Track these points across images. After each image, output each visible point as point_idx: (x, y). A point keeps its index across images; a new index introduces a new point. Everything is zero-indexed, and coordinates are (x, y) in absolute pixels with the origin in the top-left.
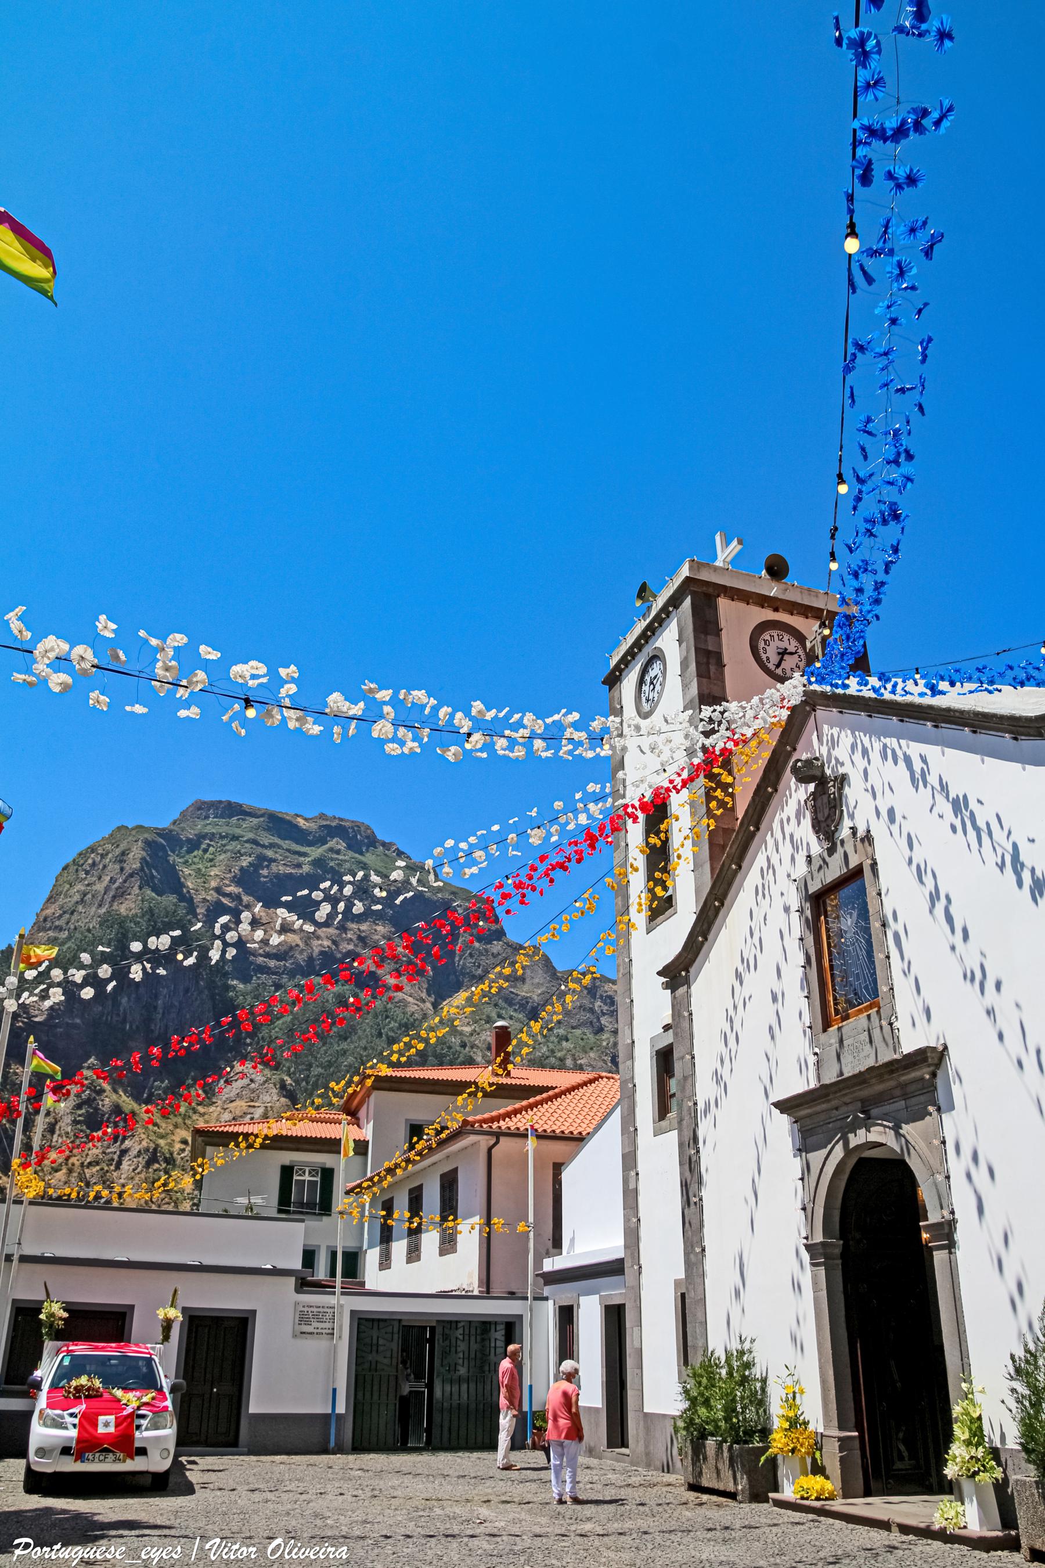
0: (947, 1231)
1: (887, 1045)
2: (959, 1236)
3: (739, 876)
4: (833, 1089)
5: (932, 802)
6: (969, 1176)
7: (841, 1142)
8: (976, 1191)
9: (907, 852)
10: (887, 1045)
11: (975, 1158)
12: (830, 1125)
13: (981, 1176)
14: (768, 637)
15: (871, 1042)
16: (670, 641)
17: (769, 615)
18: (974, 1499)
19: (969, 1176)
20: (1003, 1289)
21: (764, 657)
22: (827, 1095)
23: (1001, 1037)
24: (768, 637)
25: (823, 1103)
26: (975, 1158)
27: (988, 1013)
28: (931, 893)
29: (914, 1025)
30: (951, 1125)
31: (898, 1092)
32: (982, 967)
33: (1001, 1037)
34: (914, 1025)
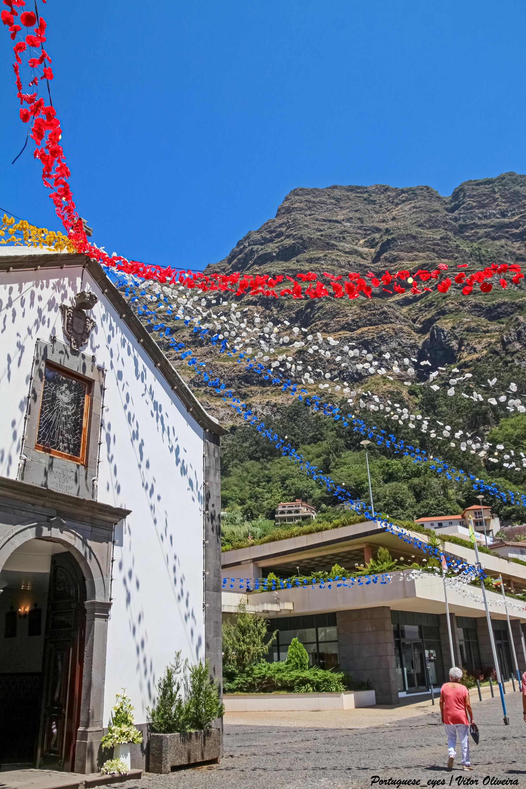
0: (105, 608)
1: (88, 490)
2: (112, 612)
3: (169, 387)
4: (53, 496)
5: (3, 328)
6: (125, 581)
7: (34, 529)
8: (127, 591)
9: (125, 402)
10: (88, 490)
11: (130, 574)
12: (24, 513)
13: (131, 585)
15: (76, 481)
18: (129, 754)
19: (125, 581)
20: (133, 644)
22: (45, 496)
23: (155, 521)
25: (11, 492)
26: (130, 574)
27: (151, 507)
28: (134, 432)
29: (108, 488)
30: (117, 552)
31: (88, 520)
32: (152, 486)
33: (155, 521)
34: (108, 488)
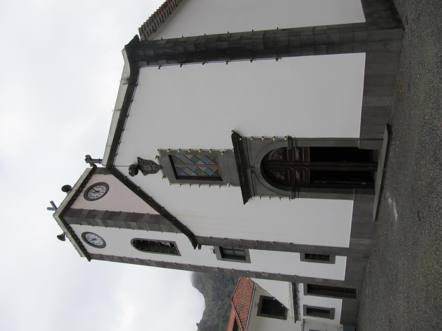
14: (90, 196)
16: (79, 229)
17: (82, 194)
21: (96, 198)
24: (90, 196)
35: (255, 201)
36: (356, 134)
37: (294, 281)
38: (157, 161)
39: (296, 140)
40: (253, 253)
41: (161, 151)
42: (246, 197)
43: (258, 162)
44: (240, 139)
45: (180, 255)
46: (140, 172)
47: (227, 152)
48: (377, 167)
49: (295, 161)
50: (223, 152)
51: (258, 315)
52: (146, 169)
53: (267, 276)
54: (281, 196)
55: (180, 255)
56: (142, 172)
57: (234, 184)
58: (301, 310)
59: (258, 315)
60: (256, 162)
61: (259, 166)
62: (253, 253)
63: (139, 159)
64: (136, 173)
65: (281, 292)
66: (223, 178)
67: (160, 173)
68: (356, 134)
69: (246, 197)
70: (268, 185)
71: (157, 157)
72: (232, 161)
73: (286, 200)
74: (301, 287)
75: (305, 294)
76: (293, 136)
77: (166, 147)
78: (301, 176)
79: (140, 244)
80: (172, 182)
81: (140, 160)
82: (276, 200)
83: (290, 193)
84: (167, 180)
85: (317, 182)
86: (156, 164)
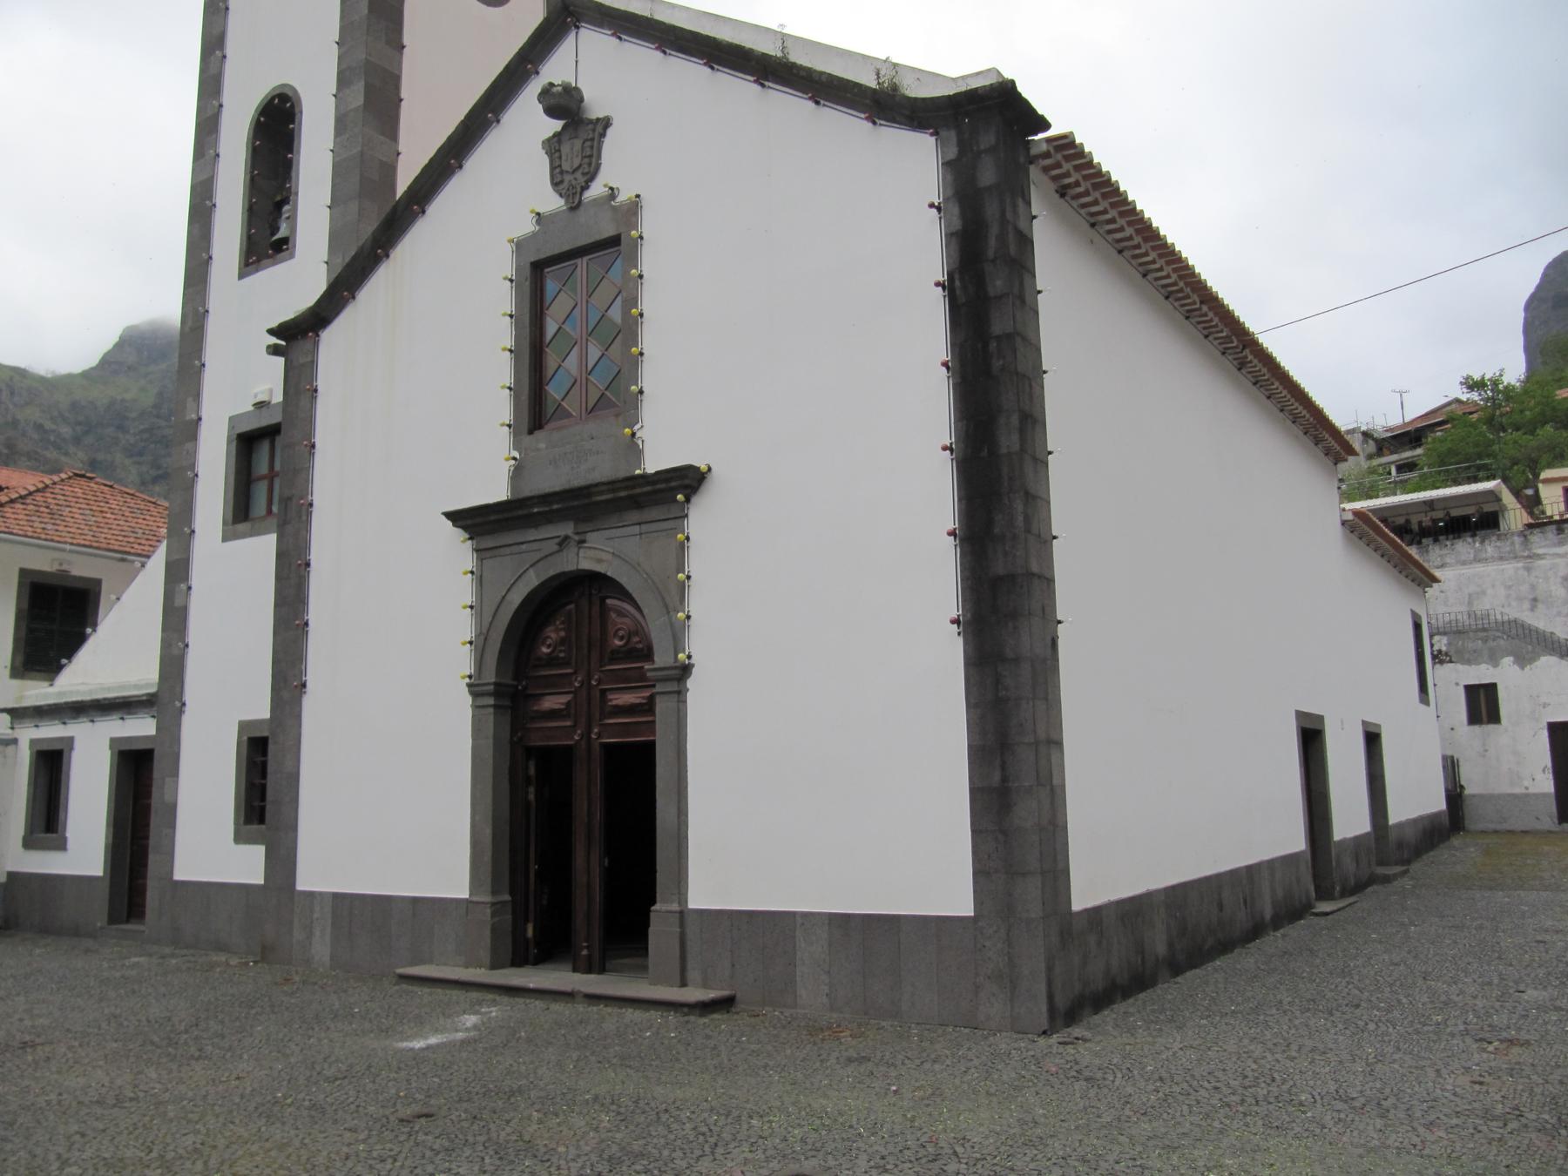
35: (458, 551)
36: (698, 898)
37: (164, 702)
38: (596, 190)
39: (680, 694)
40: (263, 548)
41: (634, 207)
42: (475, 522)
43: (600, 561)
44: (680, 497)
45: (241, 276)
46: (557, 125)
47: (633, 449)
48: (589, 971)
49: (604, 692)
50: (633, 435)
51: (24, 573)
52: (565, 149)
53: (178, 602)
54: (479, 645)
55: (241, 276)
56: (557, 135)
57: (517, 474)
58: (51, 731)
59: (24, 573)
60: (602, 551)
61: (586, 565)
62: (263, 548)
63: (606, 123)
64: (551, 112)
65: (118, 653)
66: (539, 434)
67: (553, 202)
68: (698, 898)
69: (475, 522)
70: (516, 598)
71: (613, 193)
72: (600, 468)
73: (464, 662)
74: (142, 727)
75: (113, 741)
76: (690, 683)
77: (649, 225)
78: (553, 714)
79: (277, 121)
80: (520, 246)
81: (599, 128)
82: (464, 627)
83: (490, 677)
84: (528, 227)
85: (532, 771)
86: (586, 187)
